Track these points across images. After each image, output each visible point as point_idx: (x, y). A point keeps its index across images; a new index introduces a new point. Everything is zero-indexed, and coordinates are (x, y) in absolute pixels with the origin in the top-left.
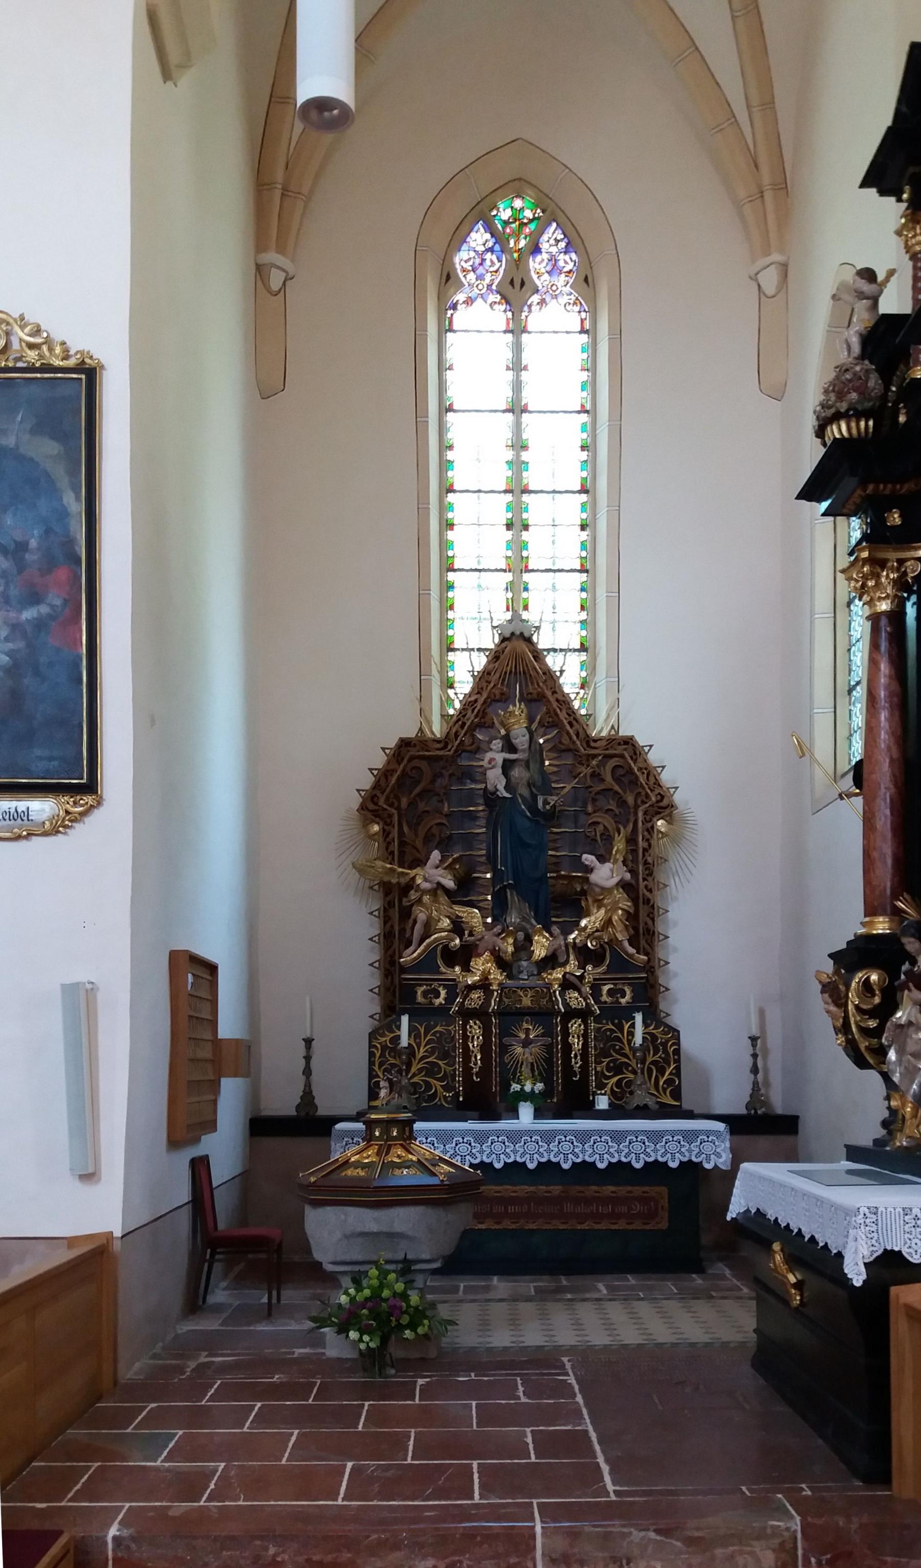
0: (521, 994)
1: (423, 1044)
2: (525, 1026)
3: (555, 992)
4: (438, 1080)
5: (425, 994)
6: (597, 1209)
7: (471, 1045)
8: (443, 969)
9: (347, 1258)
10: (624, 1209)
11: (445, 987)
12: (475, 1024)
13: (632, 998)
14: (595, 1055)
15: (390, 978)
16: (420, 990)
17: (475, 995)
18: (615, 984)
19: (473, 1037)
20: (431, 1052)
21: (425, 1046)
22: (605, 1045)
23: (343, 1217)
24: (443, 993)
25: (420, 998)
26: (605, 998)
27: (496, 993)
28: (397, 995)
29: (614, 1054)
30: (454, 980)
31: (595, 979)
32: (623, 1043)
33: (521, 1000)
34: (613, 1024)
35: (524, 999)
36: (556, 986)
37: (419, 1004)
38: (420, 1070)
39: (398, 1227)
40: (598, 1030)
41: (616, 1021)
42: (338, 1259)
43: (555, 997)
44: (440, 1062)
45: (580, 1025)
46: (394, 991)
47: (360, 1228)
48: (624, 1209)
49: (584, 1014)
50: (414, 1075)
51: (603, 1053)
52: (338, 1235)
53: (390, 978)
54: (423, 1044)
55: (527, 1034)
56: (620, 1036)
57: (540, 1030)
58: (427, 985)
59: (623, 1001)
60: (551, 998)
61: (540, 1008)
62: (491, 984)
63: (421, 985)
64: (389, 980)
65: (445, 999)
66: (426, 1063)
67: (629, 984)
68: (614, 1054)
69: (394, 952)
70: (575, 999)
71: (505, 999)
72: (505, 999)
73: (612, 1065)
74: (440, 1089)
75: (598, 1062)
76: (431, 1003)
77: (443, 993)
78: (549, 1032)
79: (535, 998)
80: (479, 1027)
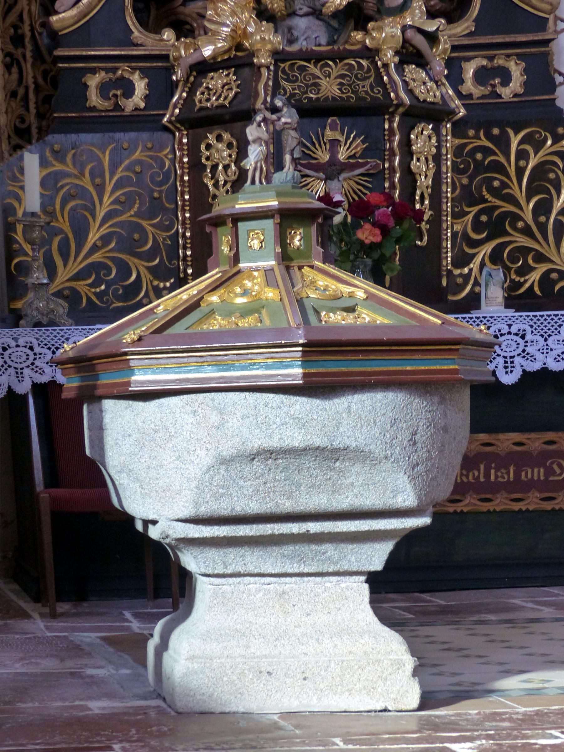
0: (317, 72)
1: (109, 188)
2: (329, 134)
3: (386, 66)
4: (139, 256)
5: (104, 89)
6: (487, 475)
7: (210, 184)
8: (137, 34)
9: (224, 508)
10: (539, 473)
11: (144, 72)
12: (219, 138)
13: (526, 84)
14: (453, 199)
15: (15, 69)
16: (93, 81)
17: (217, 81)
18: (491, 58)
19: (214, 168)
20: (124, 203)
21: (113, 192)
22: (471, 178)
23: (214, 418)
24: (141, 86)
25: (94, 99)
26: (469, 85)
27: (265, 72)
28: (32, 106)
29: (488, 196)
30: (165, 58)
31: (454, 48)
32: (509, 177)
33: (316, 85)
34: (489, 136)
35: (324, 82)
36: (390, 53)
37: (93, 109)
38: (105, 239)
39: (348, 436)
40: (458, 151)
41: (496, 131)
42: (204, 510)
43: (388, 75)
44: (144, 223)
45: (430, 137)
46: (26, 98)
47: (258, 441)
48: (539, 473)
49: (435, 114)
50: (95, 249)
51: (468, 197)
52: (205, 458)
53: (15, 69)
54: (109, 188)
55: (333, 153)
56: (502, 159)
57: (359, 146)
58: (107, 70)
59: (506, 93)
60: (379, 77)
61: (359, 98)
62: (252, 54)
63: (94, 71)
64: (15, 76)
65: (147, 98)
66: (120, 224)
67: (520, 56)
68: (488, 196)
69: (21, 16)
70: (423, 85)
71: (284, 83)
72: (284, 83)
73: (484, 218)
74: (146, 276)
75: (457, 216)
76: (117, 107)
77: (141, 86)
78: (375, 148)
79: (347, 81)
80: (230, 146)
